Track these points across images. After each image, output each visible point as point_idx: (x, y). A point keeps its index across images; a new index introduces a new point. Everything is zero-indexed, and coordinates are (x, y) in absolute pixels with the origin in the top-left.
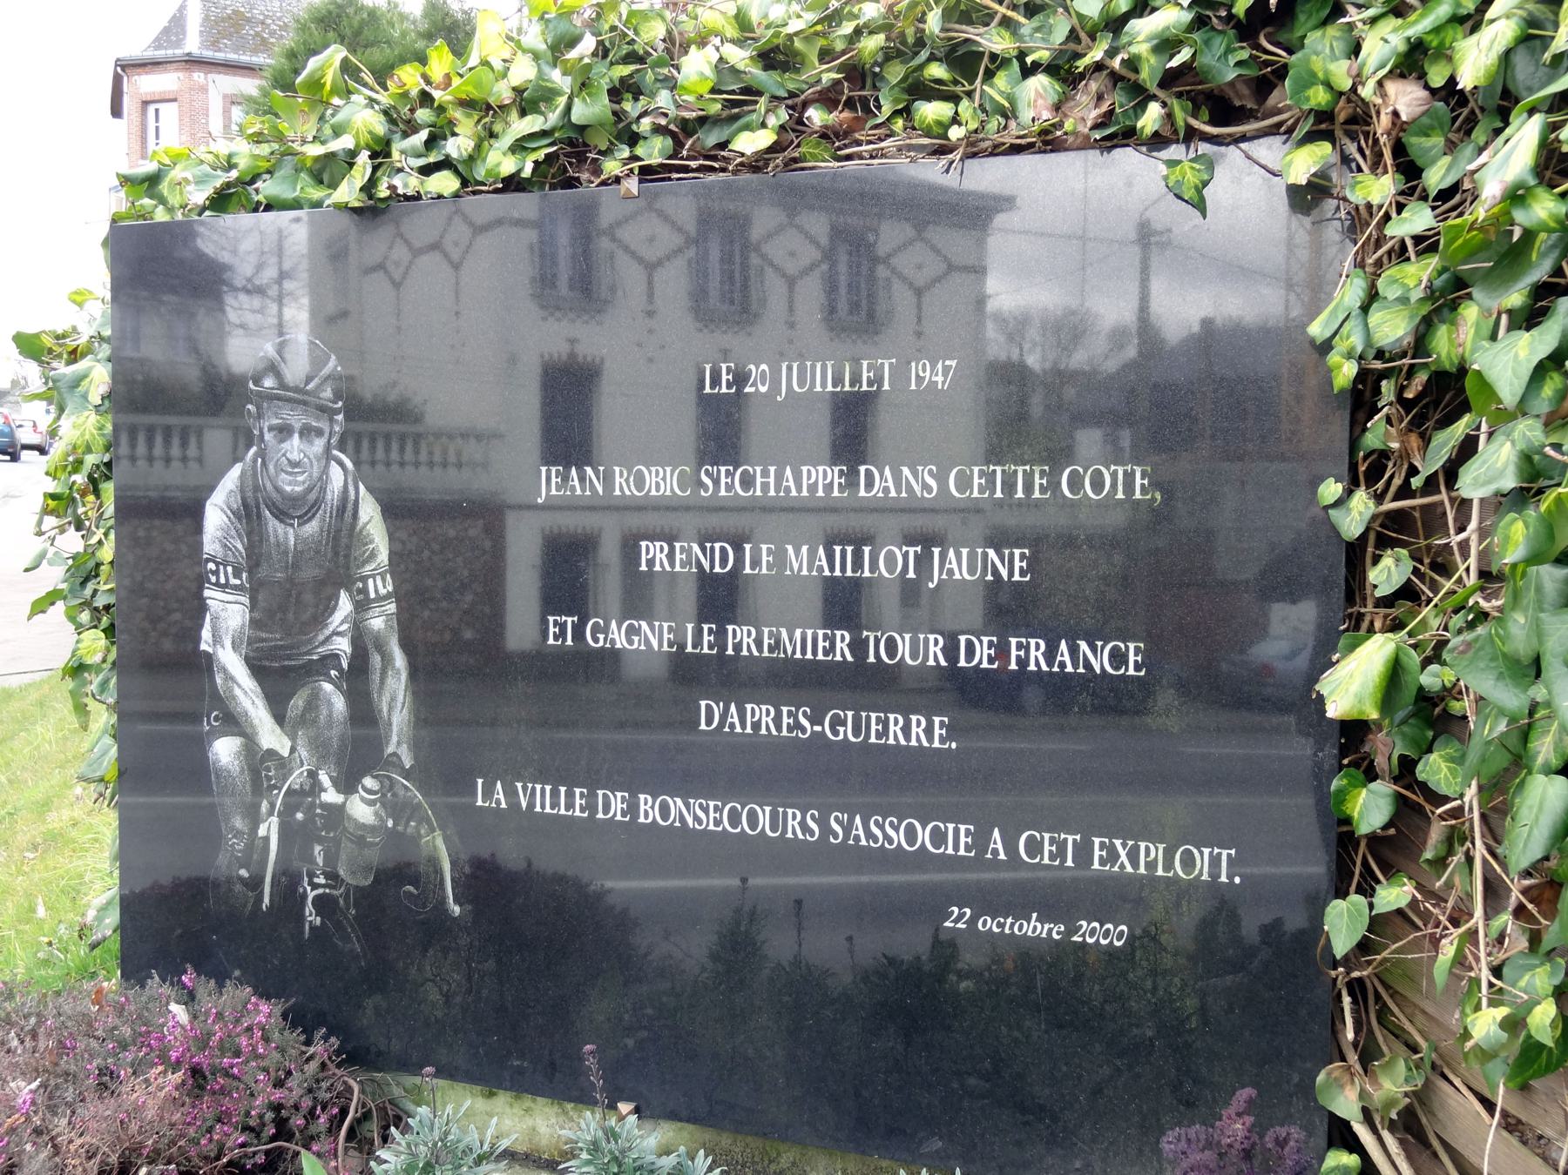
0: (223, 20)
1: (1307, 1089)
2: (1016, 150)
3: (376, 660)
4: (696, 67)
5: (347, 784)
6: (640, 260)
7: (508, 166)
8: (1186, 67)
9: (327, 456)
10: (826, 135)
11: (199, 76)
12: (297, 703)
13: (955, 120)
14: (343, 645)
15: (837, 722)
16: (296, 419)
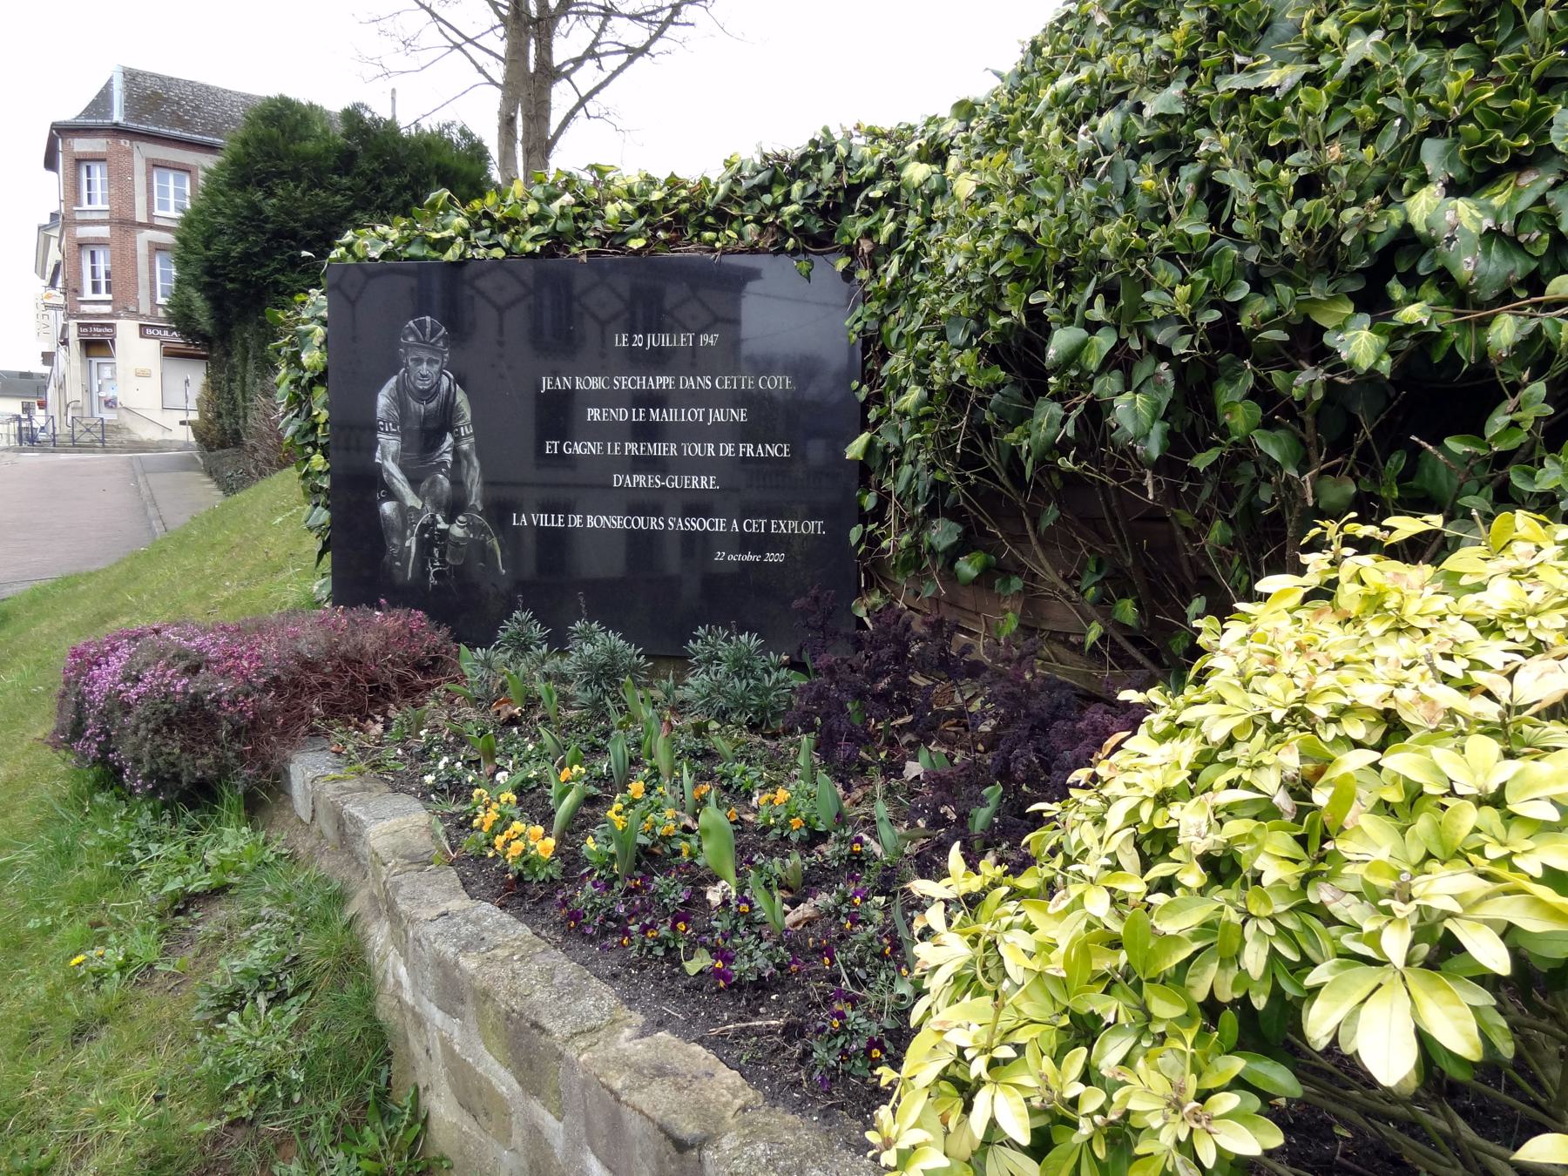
0: (144, 98)
1: (849, 609)
2: (741, 252)
3: (465, 463)
4: (612, 210)
5: (450, 520)
6: (494, 305)
7: (529, 247)
8: (802, 227)
9: (441, 372)
10: (665, 242)
11: (125, 143)
12: (425, 484)
13: (718, 239)
14: (449, 457)
15: (671, 480)
16: (425, 355)
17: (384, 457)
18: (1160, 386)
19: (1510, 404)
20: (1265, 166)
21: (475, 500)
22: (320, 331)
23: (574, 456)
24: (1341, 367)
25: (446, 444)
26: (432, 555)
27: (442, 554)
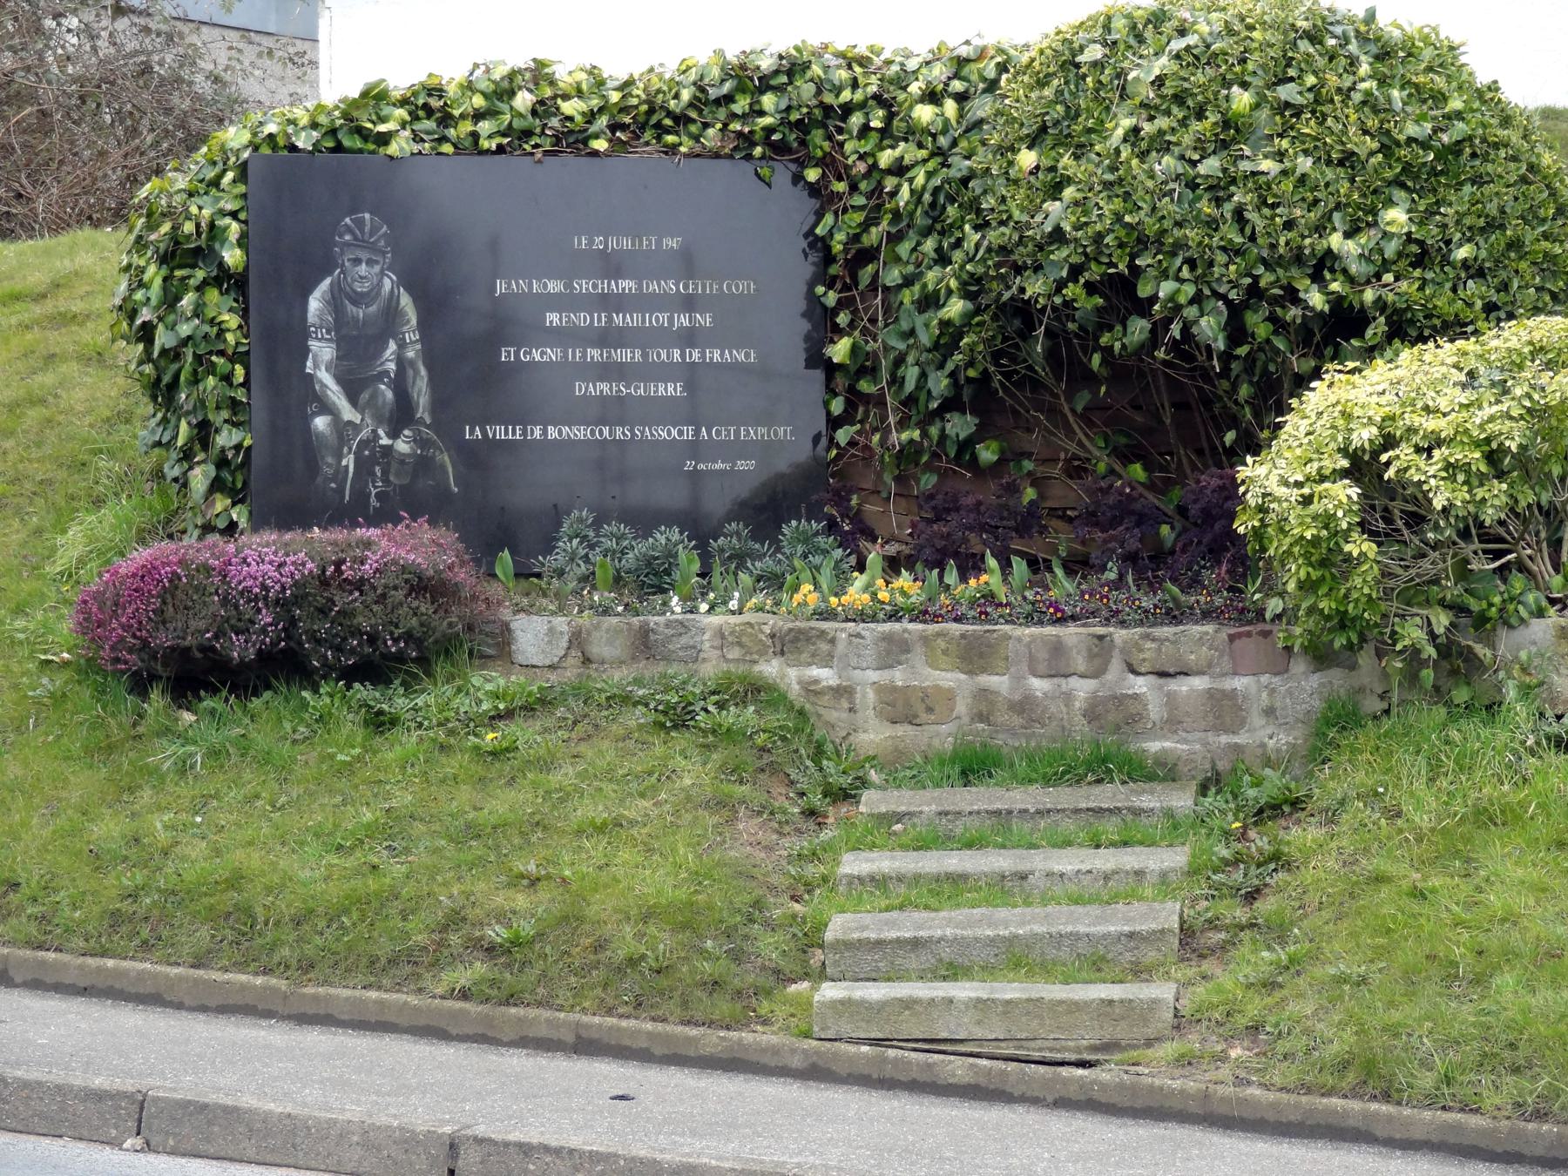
3: (410, 372)
5: (394, 434)
9: (382, 274)
12: (365, 396)
14: (392, 366)
15: (637, 388)
16: (364, 255)
17: (316, 366)
18: (1220, 313)
19: (1373, 325)
20: (1266, 211)
21: (423, 411)
22: (235, 228)
23: (533, 363)
24: (1307, 307)
25: (389, 352)
26: (374, 474)
27: (385, 473)
